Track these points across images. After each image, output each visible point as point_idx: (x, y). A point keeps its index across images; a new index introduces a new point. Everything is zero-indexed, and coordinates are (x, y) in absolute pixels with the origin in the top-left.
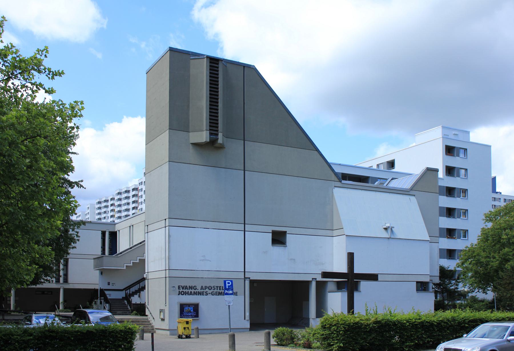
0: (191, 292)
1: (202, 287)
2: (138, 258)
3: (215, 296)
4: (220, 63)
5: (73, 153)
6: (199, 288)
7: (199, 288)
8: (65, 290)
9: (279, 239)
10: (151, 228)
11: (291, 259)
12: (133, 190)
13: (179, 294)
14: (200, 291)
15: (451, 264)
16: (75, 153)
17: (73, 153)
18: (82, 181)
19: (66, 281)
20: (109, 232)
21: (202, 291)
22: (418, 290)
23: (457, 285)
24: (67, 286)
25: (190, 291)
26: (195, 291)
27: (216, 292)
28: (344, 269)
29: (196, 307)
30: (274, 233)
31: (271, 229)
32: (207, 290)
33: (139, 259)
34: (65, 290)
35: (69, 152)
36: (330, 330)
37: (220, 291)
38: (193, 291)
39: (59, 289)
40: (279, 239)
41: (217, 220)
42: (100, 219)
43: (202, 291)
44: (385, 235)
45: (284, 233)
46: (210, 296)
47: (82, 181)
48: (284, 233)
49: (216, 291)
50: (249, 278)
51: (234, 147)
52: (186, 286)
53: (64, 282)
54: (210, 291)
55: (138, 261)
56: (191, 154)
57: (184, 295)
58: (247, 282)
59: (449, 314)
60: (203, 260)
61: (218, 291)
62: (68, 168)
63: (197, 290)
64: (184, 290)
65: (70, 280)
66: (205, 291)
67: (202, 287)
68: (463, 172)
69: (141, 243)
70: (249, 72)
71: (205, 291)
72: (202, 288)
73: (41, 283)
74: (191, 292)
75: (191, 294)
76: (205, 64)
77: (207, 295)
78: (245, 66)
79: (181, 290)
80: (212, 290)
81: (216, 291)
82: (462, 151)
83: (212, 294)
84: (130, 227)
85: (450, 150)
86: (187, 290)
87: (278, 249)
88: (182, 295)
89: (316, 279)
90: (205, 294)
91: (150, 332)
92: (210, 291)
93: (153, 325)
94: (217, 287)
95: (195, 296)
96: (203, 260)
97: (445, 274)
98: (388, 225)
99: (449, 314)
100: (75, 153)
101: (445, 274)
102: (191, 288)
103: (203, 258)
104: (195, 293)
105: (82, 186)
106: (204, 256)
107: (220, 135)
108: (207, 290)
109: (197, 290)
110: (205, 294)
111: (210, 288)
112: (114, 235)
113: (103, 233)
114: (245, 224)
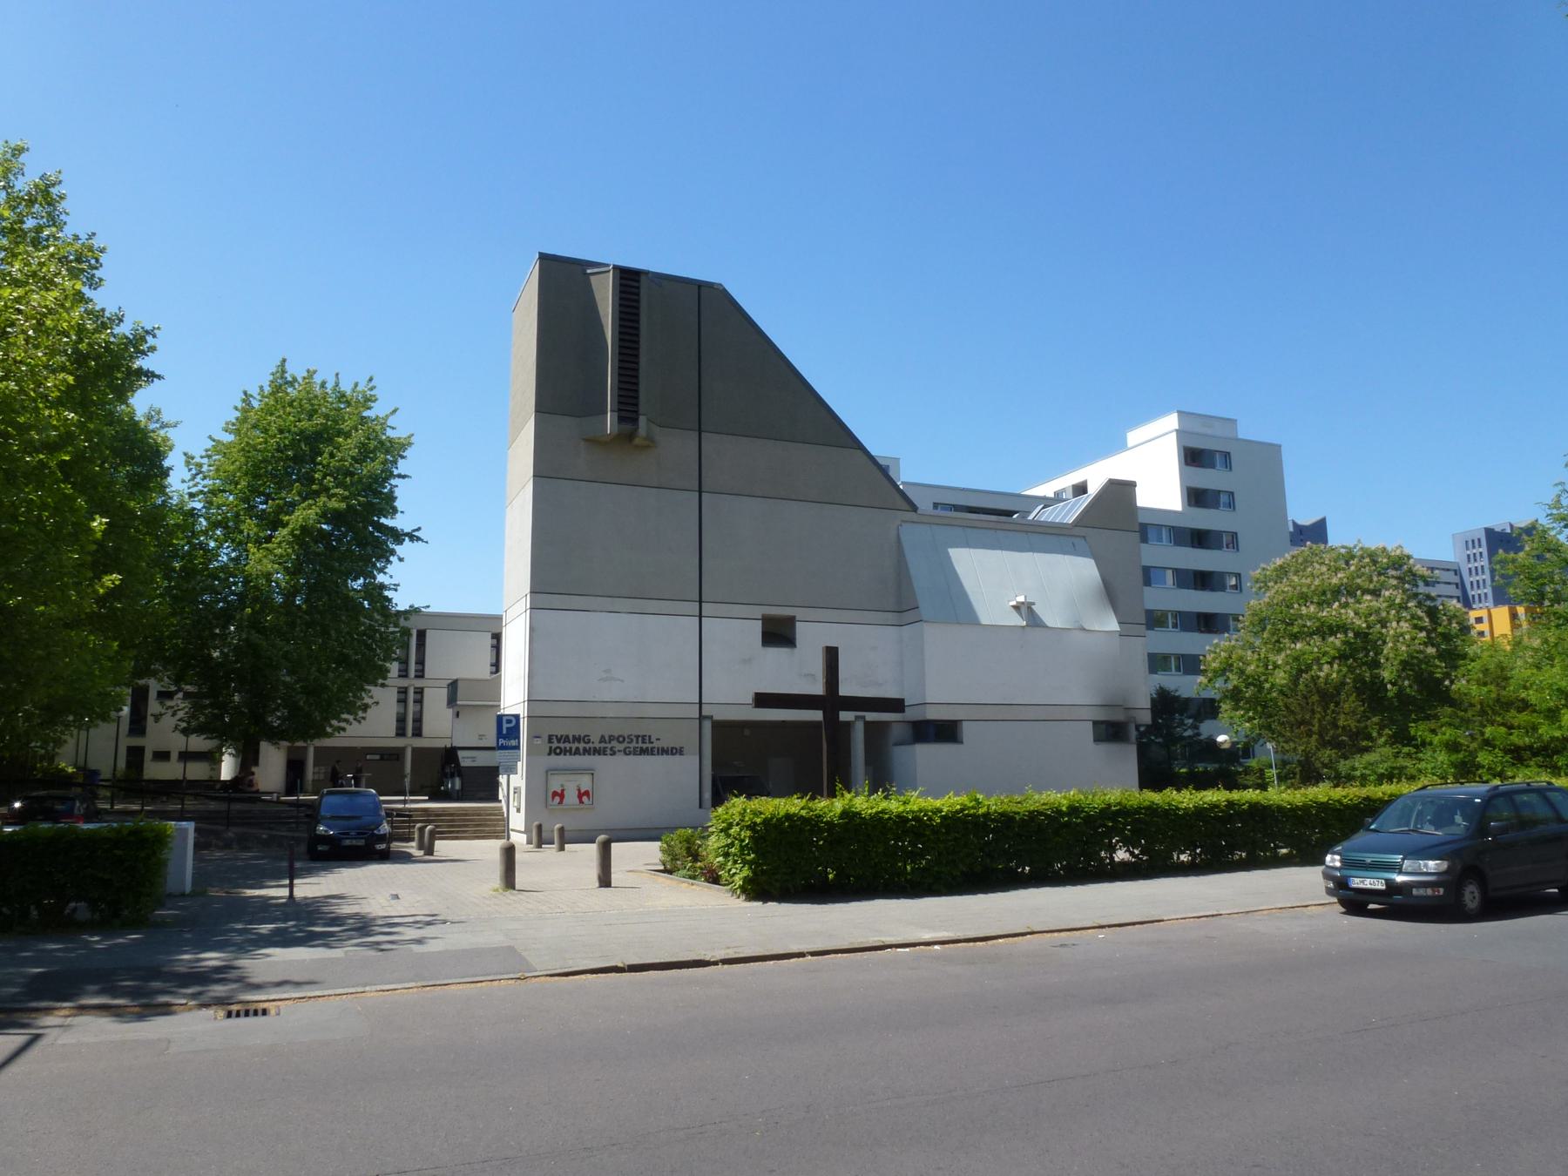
4: (643, 278)
5: (400, 476)
6: (595, 738)
7: (595, 738)
14: (597, 745)
15: (1189, 686)
16: (404, 477)
17: (400, 476)
18: (419, 529)
19: (418, 732)
22: (1098, 739)
23: (1197, 728)
28: (818, 689)
30: (767, 621)
31: (759, 611)
32: (614, 743)
35: (1464, 656)
36: (728, 836)
38: (581, 746)
41: (640, 592)
45: (791, 621)
46: (620, 758)
47: (419, 529)
48: (791, 621)
49: (634, 744)
58: (707, 725)
59: (1321, 792)
62: (388, 505)
68: (1224, 499)
72: (602, 740)
73: (330, 735)
75: (577, 752)
77: (613, 753)
78: (700, 286)
79: (555, 744)
81: (634, 744)
83: (626, 752)
85: (1193, 457)
86: (568, 745)
87: (777, 654)
97: (1165, 703)
98: (1021, 599)
99: (1321, 792)
100: (404, 477)
101: (1165, 703)
102: (577, 739)
104: (587, 752)
105: (419, 539)
107: (642, 420)
108: (614, 743)
111: (620, 739)
114: (700, 602)
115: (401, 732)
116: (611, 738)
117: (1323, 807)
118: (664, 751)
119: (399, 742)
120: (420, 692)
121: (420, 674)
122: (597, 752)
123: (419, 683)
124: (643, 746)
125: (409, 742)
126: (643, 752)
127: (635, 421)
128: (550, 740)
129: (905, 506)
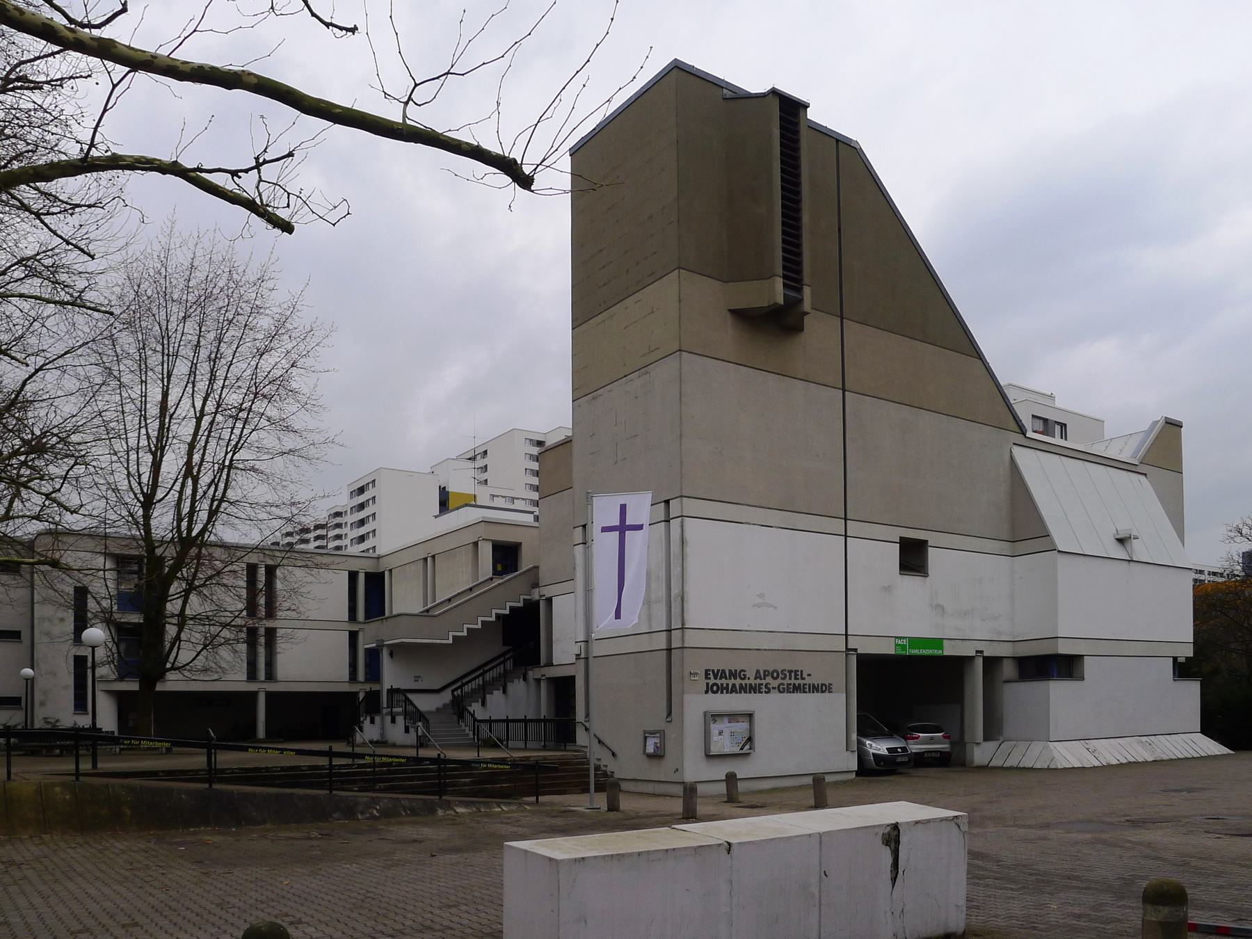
0: (734, 685)
1: (758, 671)
2: (480, 619)
3: (785, 694)
6: (751, 674)
7: (751, 674)
8: (269, 695)
9: (913, 557)
11: (938, 606)
12: (317, 527)
13: (706, 692)
14: (753, 681)
19: (270, 676)
20: (366, 574)
21: (758, 681)
24: (272, 687)
25: (731, 682)
26: (743, 682)
27: (789, 685)
32: (769, 679)
37: (797, 682)
38: (738, 682)
40: (913, 557)
43: (758, 681)
44: (1119, 552)
46: (775, 696)
49: (787, 681)
50: (856, 650)
51: (819, 330)
52: (723, 671)
54: (775, 683)
55: (465, 634)
56: (726, 334)
57: (719, 694)
60: (759, 606)
61: (793, 681)
63: (746, 681)
64: (719, 682)
66: (764, 682)
67: (758, 671)
70: (845, 152)
71: (764, 682)
74: (734, 685)
75: (733, 690)
79: (712, 681)
81: (787, 681)
82: (1058, 428)
84: (425, 559)
86: (724, 681)
87: (911, 582)
89: (982, 652)
90: (764, 689)
92: (775, 683)
93: (609, 769)
94: (790, 672)
96: (759, 606)
102: (733, 674)
104: (743, 689)
106: (761, 596)
107: (807, 291)
108: (769, 679)
109: (746, 681)
110: (764, 689)
111: (775, 674)
112: (376, 582)
113: (353, 576)
115: (252, 675)
116: (766, 673)
117: (514, 763)
118: (815, 689)
119: (252, 687)
120: (271, 633)
121: (271, 613)
122: (754, 689)
123: (270, 624)
124: (795, 683)
125: (261, 687)
126: (796, 689)
127: (799, 290)
128: (707, 677)
129: (1013, 425)
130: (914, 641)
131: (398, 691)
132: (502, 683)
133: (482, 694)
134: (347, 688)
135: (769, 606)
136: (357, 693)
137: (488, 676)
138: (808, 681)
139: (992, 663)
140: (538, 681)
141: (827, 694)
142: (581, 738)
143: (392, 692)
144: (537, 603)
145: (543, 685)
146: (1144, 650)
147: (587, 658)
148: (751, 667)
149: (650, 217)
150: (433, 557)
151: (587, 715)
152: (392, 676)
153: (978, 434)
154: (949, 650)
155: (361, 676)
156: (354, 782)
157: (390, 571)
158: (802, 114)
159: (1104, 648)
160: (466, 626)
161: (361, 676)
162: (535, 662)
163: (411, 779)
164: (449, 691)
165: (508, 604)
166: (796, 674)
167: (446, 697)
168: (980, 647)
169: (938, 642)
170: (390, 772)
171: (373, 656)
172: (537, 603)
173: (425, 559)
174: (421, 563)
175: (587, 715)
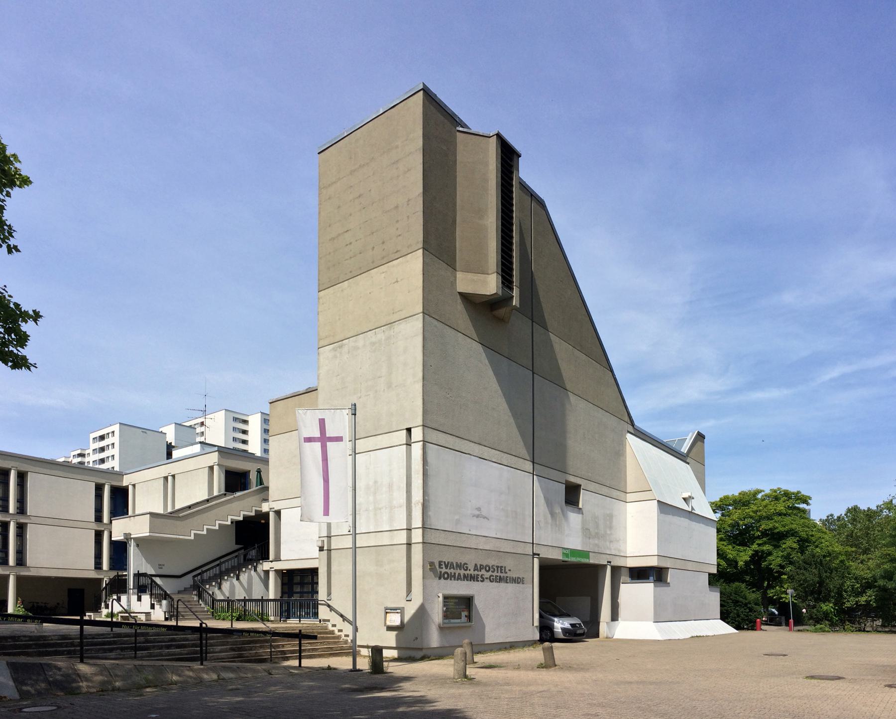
0: (459, 574)
2: (218, 522)
3: (494, 583)
6: (471, 567)
7: (471, 567)
10: (361, 445)
13: (440, 578)
24: (24, 573)
25: (458, 571)
26: (466, 573)
29: (467, 602)
32: (483, 572)
33: (207, 529)
34: (20, 580)
37: (502, 575)
38: (462, 572)
39: (7, 577)
42: (102, 461)
43: (476, 572)
46: (487, 583)
49: (495, 574)
52: (452, 563)
53: (17, 564)
55: (205, 532)
56: (460, 313)
58: (536, 561)
60: (478, 516)
61: (499, 574)
63: (468, 572)
64: (449, 571)
65: (29, 561)
69: (190, 507)
74: (459, 574)
76: (492, 146)
79: (444, 570)
80: (490, 573)
81: (495, 574)
84: (166, 478)
86: (452, 571)
88: (445, 579)
91: (347, 654)
94: (498, 567)
95: (466, 582)
96: (478, 516)
102: (459, 566)
103: (477, 513)
104: (467, 578)
106: (479, 509)
109: (468, 572)
110: (480, 579)
111: (488, 568)
113: (99, 489)
116: (482, 567)
122: (473, 578)
124: (500, 576)
126: (501, 580)
127: (511, 289)
129: (627, 418)
130: (574, 552)
131: (145, 575)
132: (236, 571)
133: (218, 578)
134: (93, 575)
135: (485, 517)
136: (100, 580)
137: (223, 567)
138: (509, 574)
139: (616, 570)
140: (267, 573)
141: (521, 585)
142: (323, 612)
143: (138, 575)
144: (267, 515)
145: (272, 575)
146: (697, 566)
147: (329, 550)
148: (470, 560)
149: (397, 207)
150: (173, 476)
151: (329, 594)
152: (136, 562)
153: (612, 421)
154: (592, 560)
155: (105, 565)
156: (111, 650)
157: (134, 486)
158: (515, 159)
159: (679, 564)
160: (205, 527)
161: (105, 565)
162: (265, 556)
163: (168, 647)
164: (190, 576)
165: (242, 513)
166: (501, 568)
167: (188, 581)
168: (609, 558)
169: (586, 554)
170: (147, 641)
171: (119, 550)
172: (267, 515)
173: (166, 478)
174: (162, 481)
175: (329, 594)
